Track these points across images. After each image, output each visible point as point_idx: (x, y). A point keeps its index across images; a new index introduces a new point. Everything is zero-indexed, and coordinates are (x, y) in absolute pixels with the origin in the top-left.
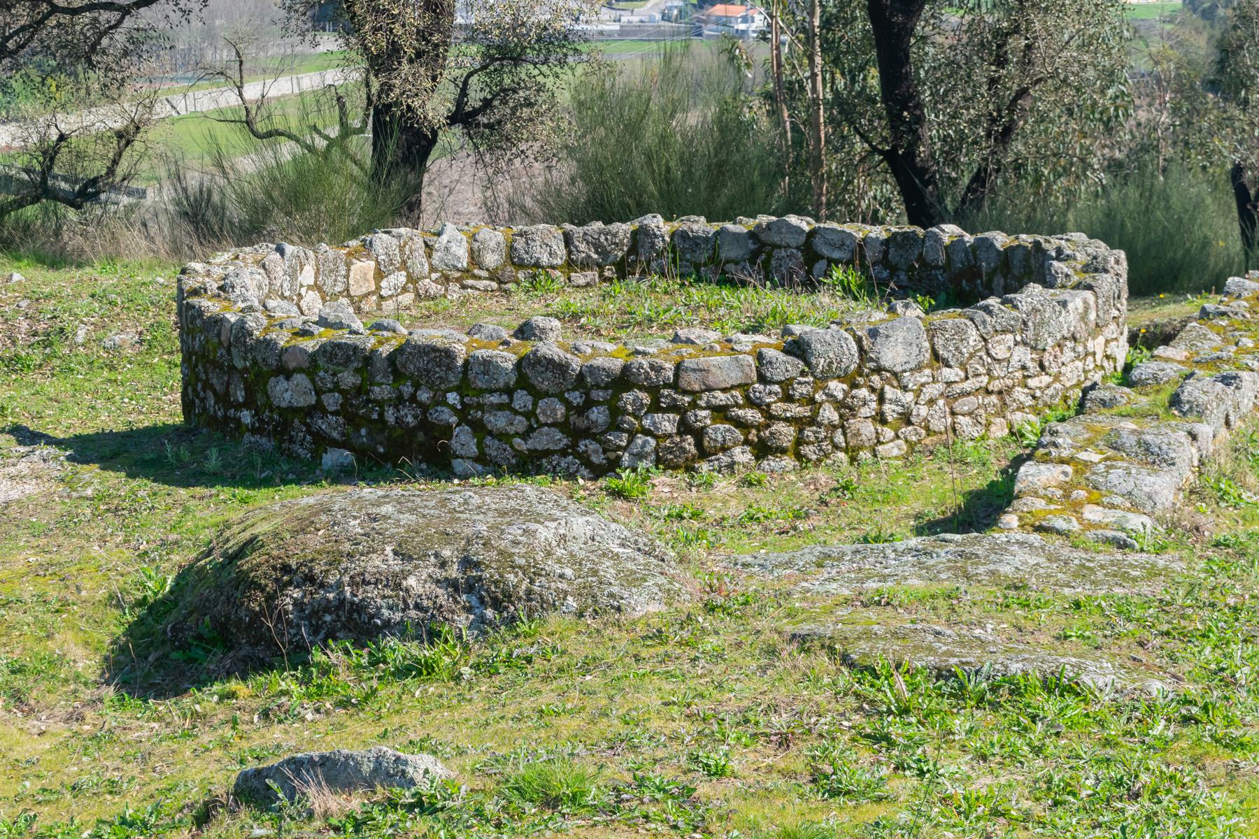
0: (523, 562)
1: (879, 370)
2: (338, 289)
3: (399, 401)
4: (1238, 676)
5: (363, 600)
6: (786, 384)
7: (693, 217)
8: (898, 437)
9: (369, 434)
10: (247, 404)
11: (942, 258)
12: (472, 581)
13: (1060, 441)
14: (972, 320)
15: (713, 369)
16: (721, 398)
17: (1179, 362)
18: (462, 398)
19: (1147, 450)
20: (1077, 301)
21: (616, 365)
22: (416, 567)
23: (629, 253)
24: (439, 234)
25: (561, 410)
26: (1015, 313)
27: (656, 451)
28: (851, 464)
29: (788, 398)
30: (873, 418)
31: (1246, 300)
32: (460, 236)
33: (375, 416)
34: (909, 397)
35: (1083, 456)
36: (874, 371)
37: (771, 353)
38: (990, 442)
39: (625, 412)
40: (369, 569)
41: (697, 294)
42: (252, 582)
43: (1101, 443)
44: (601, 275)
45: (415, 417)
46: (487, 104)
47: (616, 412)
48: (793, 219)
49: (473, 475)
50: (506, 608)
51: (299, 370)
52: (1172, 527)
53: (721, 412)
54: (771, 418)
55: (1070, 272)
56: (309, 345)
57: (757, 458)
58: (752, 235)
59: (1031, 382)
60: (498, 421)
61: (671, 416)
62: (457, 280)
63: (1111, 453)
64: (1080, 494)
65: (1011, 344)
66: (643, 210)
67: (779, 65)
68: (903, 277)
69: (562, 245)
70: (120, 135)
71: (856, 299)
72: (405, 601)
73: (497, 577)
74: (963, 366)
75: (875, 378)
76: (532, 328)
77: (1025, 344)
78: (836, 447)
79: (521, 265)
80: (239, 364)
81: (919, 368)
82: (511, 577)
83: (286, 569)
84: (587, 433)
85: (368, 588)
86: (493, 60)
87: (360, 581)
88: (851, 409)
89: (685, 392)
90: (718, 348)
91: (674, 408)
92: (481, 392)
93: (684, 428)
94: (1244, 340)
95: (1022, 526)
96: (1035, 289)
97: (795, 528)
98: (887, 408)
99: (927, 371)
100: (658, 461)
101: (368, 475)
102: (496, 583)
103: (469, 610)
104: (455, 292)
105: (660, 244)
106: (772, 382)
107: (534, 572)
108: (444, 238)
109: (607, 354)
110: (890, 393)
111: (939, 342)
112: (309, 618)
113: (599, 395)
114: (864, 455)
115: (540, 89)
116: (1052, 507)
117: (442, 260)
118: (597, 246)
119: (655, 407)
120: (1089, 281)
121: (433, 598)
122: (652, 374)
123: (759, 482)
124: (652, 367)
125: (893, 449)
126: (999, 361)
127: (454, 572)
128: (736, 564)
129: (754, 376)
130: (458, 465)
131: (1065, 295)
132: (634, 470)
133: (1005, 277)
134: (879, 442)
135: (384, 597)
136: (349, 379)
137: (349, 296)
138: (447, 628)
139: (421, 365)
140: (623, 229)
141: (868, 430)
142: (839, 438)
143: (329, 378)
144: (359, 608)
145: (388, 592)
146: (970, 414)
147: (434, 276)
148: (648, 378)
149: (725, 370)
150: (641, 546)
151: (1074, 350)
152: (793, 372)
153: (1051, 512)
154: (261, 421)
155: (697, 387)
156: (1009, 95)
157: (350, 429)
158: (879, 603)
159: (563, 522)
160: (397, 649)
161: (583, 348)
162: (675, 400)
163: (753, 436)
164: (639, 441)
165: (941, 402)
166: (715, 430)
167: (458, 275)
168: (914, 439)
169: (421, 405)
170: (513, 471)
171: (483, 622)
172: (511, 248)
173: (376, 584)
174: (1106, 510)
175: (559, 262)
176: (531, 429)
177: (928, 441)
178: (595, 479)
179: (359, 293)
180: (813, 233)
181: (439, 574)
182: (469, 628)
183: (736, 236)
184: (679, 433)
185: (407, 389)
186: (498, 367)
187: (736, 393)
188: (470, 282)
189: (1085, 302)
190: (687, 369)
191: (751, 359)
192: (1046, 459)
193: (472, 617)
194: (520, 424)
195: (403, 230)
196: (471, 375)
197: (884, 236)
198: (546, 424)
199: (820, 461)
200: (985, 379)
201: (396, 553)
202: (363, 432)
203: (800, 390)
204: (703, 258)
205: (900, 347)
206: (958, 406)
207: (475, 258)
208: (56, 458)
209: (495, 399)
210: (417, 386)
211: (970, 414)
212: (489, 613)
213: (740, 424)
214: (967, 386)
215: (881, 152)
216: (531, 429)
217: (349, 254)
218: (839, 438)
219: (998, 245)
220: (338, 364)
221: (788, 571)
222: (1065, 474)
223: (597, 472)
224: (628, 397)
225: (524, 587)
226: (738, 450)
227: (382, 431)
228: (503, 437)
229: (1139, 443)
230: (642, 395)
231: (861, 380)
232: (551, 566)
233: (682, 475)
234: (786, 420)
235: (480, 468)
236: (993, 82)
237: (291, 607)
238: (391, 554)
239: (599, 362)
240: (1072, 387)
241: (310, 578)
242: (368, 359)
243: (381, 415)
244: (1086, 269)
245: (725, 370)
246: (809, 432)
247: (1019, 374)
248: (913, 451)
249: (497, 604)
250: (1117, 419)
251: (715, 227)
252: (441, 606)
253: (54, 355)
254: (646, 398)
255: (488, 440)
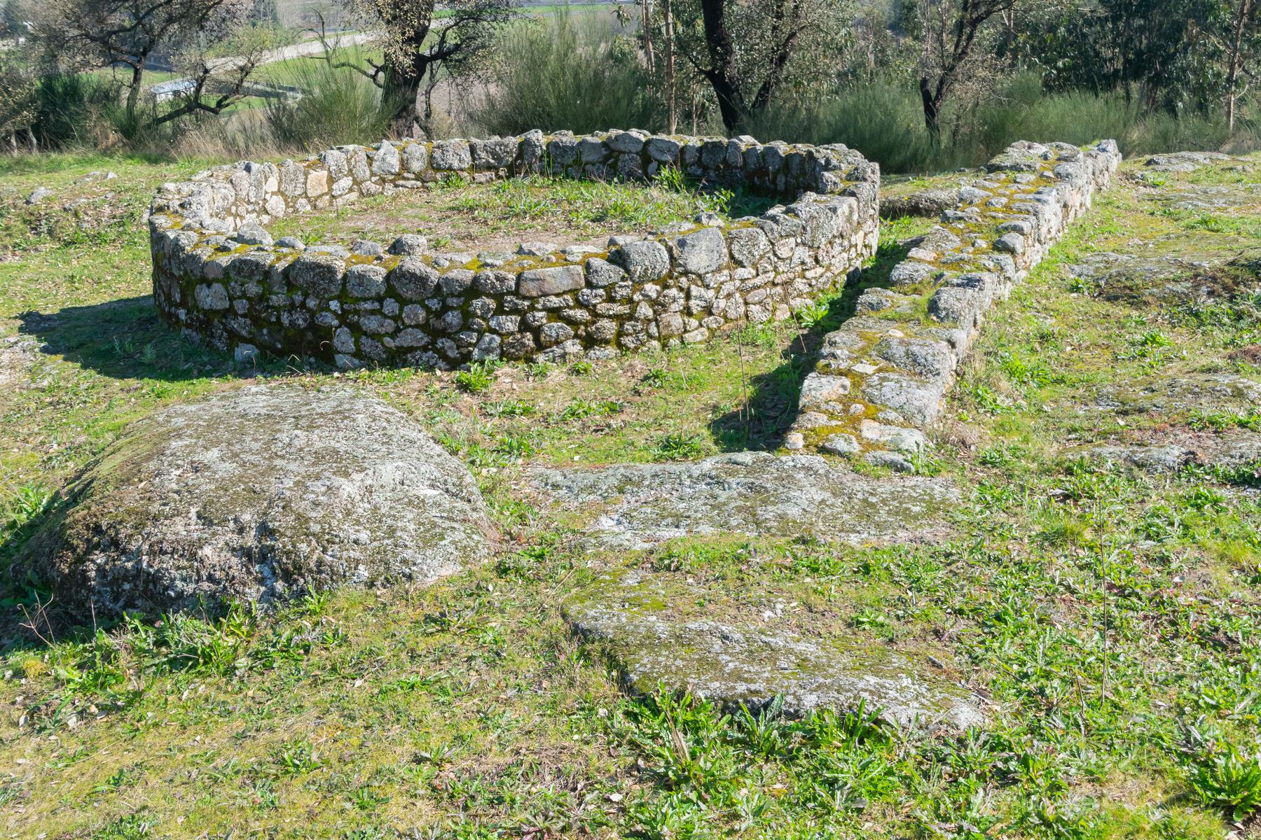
0: (316, 528)
1: (686, 273)
2: (297, 193)
3: (292, 308)
4: (1048, 691)
5: (158, 571)
6: (609, 289)
7: (564, 132)
8: (701, 325)
9: (269, 333)
10: (183, 304)
11: (740, 161)
12: (265, 551)
13: (838, 352)
14: (762, 228)
15: (548, 279)
16: (555, 301)
17: (930, 263)
18: (342, 305)
19: (915, 361)
20: (845, 205)
21: (467, 276)
22: (214, 534)
23: (516, 159)
24: (378, 149)
25: (422, 314)
26: (796, 221)
27: (501, 346)
28: (663, 350)
29: (611, 299)
30: (681, 312)
31: (977, 206)
32: (394, 149)
33: (273, 319)
34: (711, 293)
35: (859, 368)
36: (681, 274)
37: (597, 263)
38: (776, 324)
39: (475, 315)
40: (169, 536)
41: (561, 191)
42: (67, 542)
43: (874, 353)
44: (497, 175)
45: (305, 320)
46: (457, 47)
47: (467, 315)
48: (634, 133)
49: (350, 369)
50: (296, 581)
51: (217, 280)
52: (942, 441)
53: (555, 313)
54: (596, 316)
55: (838, 180)
56: (224, 260)
57: (586, 348)
58: (605, 145)
59: (808, 274)
60: (371, 324)
61: (513, 317)
62: (391, 181)
63: (883, 363)
64: (857, 408)
65: (793, 245)
66: (525, 129)
67: (647, 19)
68: (712, 173)
69: (468, 154)
70: (242, 69)
71: (677, 191)
72: (198, 573)
73: (289, 547)
74: (755, 266)
75: (683, 279)
76: (402, 245)
77: (804, 244)
78: (651, 337)
79: (439, 169)
80: (176, 273)
81: (719, 270)
82: (303, 547)
83: (97, 529)
84: (443, 333)
85: (165, 558)
86: (462, 19)
87: (157, 551)
88: (663, 306)
89: (525, 298)
90: (554, 259)
91: (515, 311)
92: (358, 300)
93: (525, 326)
94: (979, 241)
95: (807, 446)
96: (811, 196)
97: (609, 426)
98: (692, 303)
99: (726, 272)
100: (502, 355)
101: (269, 367)
102: (288, 553)
103: (261, 581)
104: (390, 189)
105: (539, 152)
106: (597, 287)
107: (327, 540)
108: (382, 151)
109: (459, 264)
110: (695, 291)
111: (735, 247)
112: (110, 584)
113: (453, 302)
114: (674, 342)
115: (491, 36)
116: (834, 423)
117: (379, 168)
118: (494, 154)
119: (500, 311)
120: (852, 188)
121: (225, 569)
122: (497, 284)
123: (585, 370)
124: (497, 278)
125: (696, 336)
126: (783, 260)
127: (250, 540)
128: (546, 484)
129: (583, 283)
130: (341, 360)
131: (835, 201)
132: (482, 363)
133: (786, 176)
134: (686, 331)
135: (178, 568)
136: (253, 289)
137: (307, 197)
138: (237, 602)
139: (309, 279)
140: (513, 141)
141: (677, 321)
142: (653, 329)
143: (238, 288)
144: (155, 579)
145: (183, 563)
146: (760, 303)
147: (374, 179)
148: (493, 287)
149: (557, 278)
150: (450, 487)
151: (841, 245)
152: (615, 278)
153: (832, 430)
154: (192, 319)
155: (534, 294)
156: (784, 37)
157: (254, 330)
158: (668, 568)
159: (370, 472)
160: (187, 629)
161: (442, 262)
162: (516, 304)
163: (582, 331)
164: (487, 339)
165: (738, 295)
166: (550, 328)
167: (391, 177)
168: (715, 326)
169: (309, 310)
170: (382, 365)
171: (273, 595)
172: (431, 157)
173: (172, 553)
174: (883, 427)
175: (466, 166)
176: (398, 330)
177: (725, 327)
178: (450, 370)
179: (315, 194)
180: (648, 142)
181: (236, 540)
182: (259, 601)
183: (593, 145)
184: (520, 331)
185: (298, 298)
186: (370, 280)
187: (567, 297)
188: (401, 182)
189: (850, 207)
190: (526, 280)
191: (580, 269)
192: (827, 371)
193: (263, 589)
194: (389, 325)
195: (351, 147)
196: (349, 287)
197: (699, 144)
198: (410, 326)
199: (637, 348)
200: (772, 275)
201: (199, 516)
202: (265, 331)
203: (621, 293)
204: (570, 161)
205: (703, 255)
206: (750, 298)
207: (404, 165)
208: (32, 350)
209: (368, 306)
210: (306, 295)
211: (760, 303)
212: (280, 586)
213: (570, 321)
214: (758, 281)
215: (704, 72)
216: (398, 330)
217: (309, 166)
218: (653, 329)
219: (781, 153)
220: (245, 277)
221: (591, 497)
222: (844, 387)
223: (453, 365)
224: (477, 303)
225: (315, 558)
226: (569, 343)
227: (279, 331)
228: (375, 336)
229: (907, 354)
230: (488, 301)
231: (671, 282)
232: (348, 531)
233: (522, 365)
234: (609, 317)
235: (356, 361)
236: (775, 28)
237: (93, 574)
238: (194, 518)
239: (453, 274)
240: (839, 274)
241: (115, 543)
242: (266, 273)
243: (278, 318)
244: (850, 177)
245: (557, 278)
246: (628, 326)
247: (799, 269)
248: (714, 336)
249: (287, 577)
250: (885, 323)
251: (578, 139)
252: (234, 578)
253: (125, 232)
254: (492, 304)
255: (363, 339)
